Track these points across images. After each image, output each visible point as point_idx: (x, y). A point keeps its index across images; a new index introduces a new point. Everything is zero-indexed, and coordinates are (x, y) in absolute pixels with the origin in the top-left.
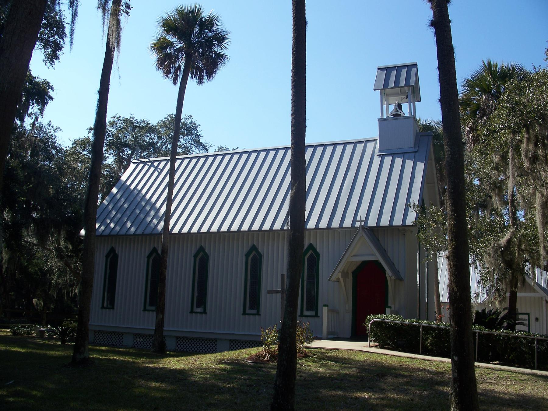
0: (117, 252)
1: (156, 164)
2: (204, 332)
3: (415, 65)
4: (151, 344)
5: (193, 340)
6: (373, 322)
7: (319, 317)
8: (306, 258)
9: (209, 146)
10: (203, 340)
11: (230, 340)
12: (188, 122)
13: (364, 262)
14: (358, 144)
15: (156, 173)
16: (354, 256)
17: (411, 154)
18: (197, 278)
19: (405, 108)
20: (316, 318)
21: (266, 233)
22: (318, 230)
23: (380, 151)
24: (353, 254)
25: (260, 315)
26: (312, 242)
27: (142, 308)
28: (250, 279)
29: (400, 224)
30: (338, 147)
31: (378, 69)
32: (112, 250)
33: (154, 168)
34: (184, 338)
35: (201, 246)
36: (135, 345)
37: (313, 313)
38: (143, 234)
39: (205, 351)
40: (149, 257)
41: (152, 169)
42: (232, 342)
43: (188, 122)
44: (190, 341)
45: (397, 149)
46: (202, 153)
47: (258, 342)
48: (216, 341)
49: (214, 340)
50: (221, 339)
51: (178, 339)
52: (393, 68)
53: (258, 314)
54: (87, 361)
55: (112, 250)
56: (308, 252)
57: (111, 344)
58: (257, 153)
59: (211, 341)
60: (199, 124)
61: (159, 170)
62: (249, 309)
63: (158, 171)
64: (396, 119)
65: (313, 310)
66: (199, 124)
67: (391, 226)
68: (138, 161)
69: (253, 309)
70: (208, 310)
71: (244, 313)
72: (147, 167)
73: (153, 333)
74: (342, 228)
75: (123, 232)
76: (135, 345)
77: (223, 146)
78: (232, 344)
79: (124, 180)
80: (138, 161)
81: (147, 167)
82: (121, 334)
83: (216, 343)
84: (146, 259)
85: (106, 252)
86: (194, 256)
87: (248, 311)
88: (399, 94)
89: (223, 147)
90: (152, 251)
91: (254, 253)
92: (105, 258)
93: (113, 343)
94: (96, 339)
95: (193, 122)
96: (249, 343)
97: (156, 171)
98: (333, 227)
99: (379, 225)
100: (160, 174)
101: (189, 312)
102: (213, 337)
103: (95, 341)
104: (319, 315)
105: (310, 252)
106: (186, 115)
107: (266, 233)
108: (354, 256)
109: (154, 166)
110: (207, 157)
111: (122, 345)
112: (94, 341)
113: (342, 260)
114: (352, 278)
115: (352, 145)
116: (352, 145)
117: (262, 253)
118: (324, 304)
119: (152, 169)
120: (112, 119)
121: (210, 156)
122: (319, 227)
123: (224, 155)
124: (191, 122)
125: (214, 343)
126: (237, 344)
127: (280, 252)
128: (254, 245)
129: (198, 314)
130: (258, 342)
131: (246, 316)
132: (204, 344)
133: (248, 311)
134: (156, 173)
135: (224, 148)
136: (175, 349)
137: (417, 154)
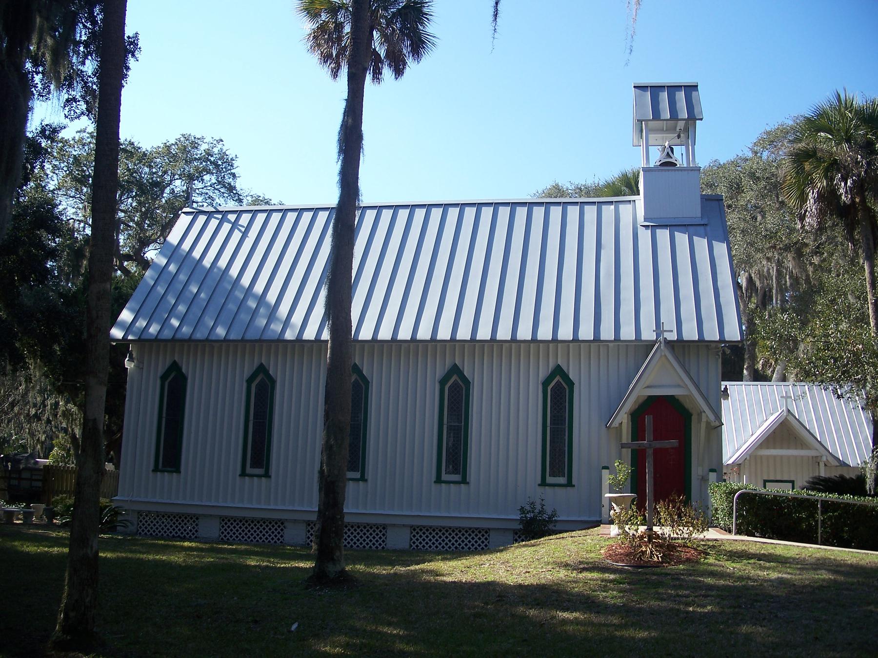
0: (184, 371)
1: (232, 217)
2: (183, 504)
3: (695, 87)
4: (346, 536)
5: (252, 522)
6: (739, 496)
7: (574, 486)
8: (269, 384)
9: (245, 195)
10: (352, 527)
11: (411, 527)
12: (216, 150)
13: (650, 397)
14: (400, 210)
15: (237, 236)
16: (648, 387)
17: (698, 228)
18: (252, 418)
19: (679, 152)
20: (569, 488)
21: (366, 345)
22: (393, 344)
23: (646, 220)
24: (647, 383)
25: (366, 481)
26: (559, 363)
27: (239, 471)
28: (254, 419)
29: (369, 337)
30: (321, 213)
31: (634, 87)
32: (175, 367)
33: (231, 225)
34: (264, 520)
35: (175, 360)
36: (222, 536)
37: (562, 480)
38: (243, 340)
39: (274, 541)
40: (250, 381)
41: (227, 227)
42: (223, 520)
43: (216, 150)
44: (246, 525)
45: (675, 218)
46: (231, 205)
47: (177, 515)
48: (197, 519)
49: (261, 520)
50: (394, 525)
51: (309, 525)
52: (661, 88)
53: (267, 475)
54: (345, 580)
55: (175, 367)
56: (451, 378)
57: (173, 535)
58: (282, 214)
59: (183, 518)
60: (236, 155)
61: (243, 230)
62: (250, 468)
63: (240, 231)
64: (662, 170)
65: (560, 474)
66: (236, 155)
67: (299, 341)
68: (194, 211)
69: (453, 473)
70: (369, 475)
71: (243, 474)
72: (214, 223)
73: (314, 517)
74: (620, 340)
75: (167, 334)
76: (222, 536)
77: (259, 195)
78: (414, 533)
79: (175, 242)
80: (194, 211)
81: (214, 223)
82: (195, 518)
83: (197, 522)
84: (245, 385)
85: (161, 371)
86: (247, 381)
87: (249, 470)
88: (663, 130)
89: (260, 197)
90: (448, 372)
91: (454, 377)
92: (159, 382)
93: (176, 533)
94: (140, 527)
95: (224, 151)
96: (180, 518)
97: (236, 230)
98: (307, 339)
99: (515, 338)
100: (245, 235)
101: (151, 469)
102: (387, 521)
103: (140, 530)
104: (573, 483)
105: (454, 377)
106: (213, 138)
107: (366, 345)
108: (648, 387)
109: (229, 221)
110: (240, 213)
111: (196, 537)
112: (138, 530)
113: (629, 396)
114: (631, 423)
115: (265, 215)
116: (265, 215)
117: (274, 377)
118: (604, 465)
119: (227, 227)
120: (78, 134)
121: (274, 211)
122: (360, 339)
123: (270, 212)
124: (220, 150)
125: (194, 522)
126: (172, 520)
127: (428, 379)
128: (262, 364)
129: (255, 478)
130: (374, 526)
131: (443, 485)
132: (243, 528)
133: (550, 480)
134: (237, 236)
135: (261, 198)
136: (304, 543)
137: (708, 228)
